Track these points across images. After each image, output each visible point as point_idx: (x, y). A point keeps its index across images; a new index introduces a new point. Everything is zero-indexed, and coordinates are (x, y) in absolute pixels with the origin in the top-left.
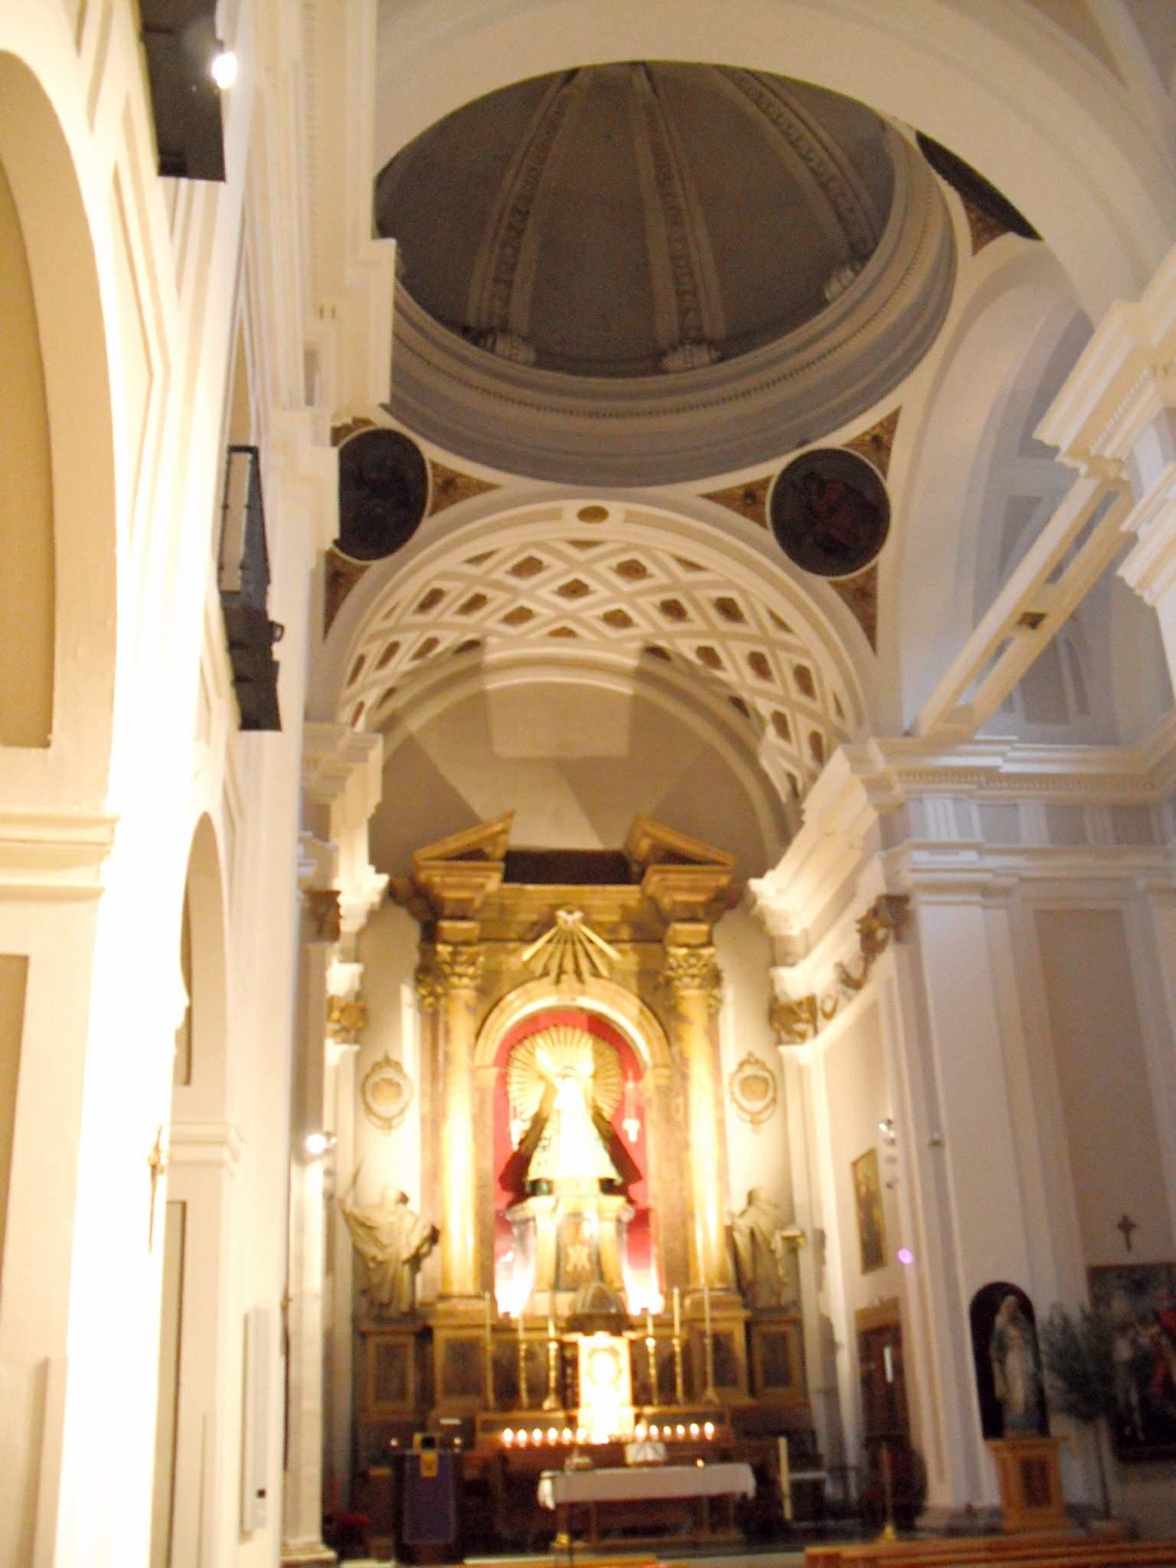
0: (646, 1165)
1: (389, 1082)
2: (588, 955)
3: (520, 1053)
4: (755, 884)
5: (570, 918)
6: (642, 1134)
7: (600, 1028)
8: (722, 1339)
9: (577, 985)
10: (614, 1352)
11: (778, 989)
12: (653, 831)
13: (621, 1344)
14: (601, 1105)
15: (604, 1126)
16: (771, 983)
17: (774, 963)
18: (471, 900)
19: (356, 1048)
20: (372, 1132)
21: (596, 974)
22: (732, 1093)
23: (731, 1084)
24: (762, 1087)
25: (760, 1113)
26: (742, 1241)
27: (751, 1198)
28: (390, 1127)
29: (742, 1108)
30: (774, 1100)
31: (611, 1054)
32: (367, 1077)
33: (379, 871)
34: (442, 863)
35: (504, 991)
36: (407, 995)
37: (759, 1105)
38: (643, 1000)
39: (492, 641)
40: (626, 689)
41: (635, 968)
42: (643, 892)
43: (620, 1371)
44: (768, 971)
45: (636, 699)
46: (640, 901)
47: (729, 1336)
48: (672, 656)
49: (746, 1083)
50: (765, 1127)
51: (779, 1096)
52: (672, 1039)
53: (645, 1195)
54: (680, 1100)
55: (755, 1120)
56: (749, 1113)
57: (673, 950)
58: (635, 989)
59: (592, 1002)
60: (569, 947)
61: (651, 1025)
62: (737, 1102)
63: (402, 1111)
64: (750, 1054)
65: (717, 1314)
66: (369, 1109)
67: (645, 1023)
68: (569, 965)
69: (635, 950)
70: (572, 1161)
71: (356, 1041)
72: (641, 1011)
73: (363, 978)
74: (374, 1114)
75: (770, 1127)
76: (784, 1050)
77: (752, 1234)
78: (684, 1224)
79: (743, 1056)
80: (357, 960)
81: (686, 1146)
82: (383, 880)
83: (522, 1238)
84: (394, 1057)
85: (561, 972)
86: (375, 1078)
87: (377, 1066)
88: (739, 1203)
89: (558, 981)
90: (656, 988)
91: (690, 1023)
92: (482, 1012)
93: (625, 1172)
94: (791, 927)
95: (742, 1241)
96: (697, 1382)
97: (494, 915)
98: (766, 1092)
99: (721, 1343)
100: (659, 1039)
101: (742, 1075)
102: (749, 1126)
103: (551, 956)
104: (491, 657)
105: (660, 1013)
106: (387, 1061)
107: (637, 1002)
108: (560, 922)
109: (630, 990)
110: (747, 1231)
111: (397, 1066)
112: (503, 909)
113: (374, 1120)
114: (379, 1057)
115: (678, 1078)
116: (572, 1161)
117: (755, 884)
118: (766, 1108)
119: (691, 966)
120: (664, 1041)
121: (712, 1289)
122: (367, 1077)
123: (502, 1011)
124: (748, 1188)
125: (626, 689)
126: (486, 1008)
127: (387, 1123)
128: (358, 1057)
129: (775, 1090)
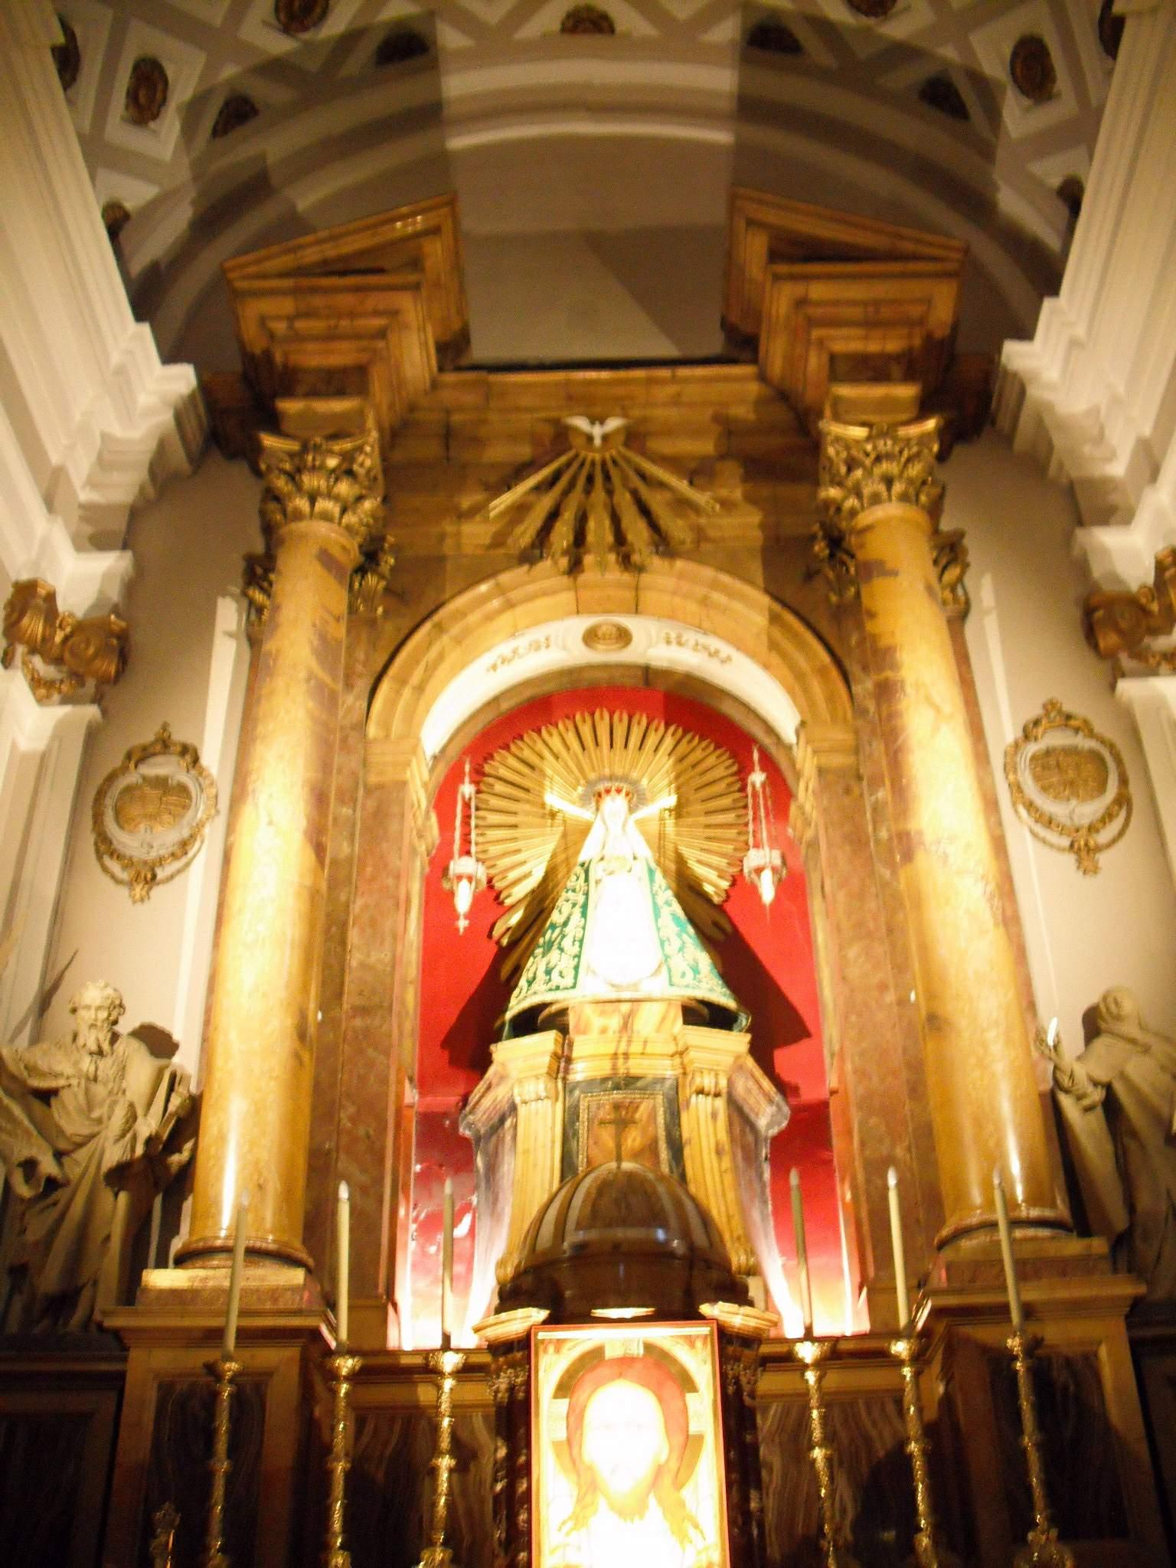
0: (814, 1000)
1: (161, 783)
2: (645, 511)
3: (504, 765)
4: (1015, 354)
5: (597, 431)
6: (793, 886)
7: (692, 711)
8: (1060, 1376)
9: (615, 574)
10: (663, 1373)
11: (1097, 572)
12: (772, 217)
13: (690, 1348)
14: (700, 870)
15: (705, 914)
16: (1081, 568)
17: (1080, 523)
18: (262, 157)
19: (92, 711)
20: (104, 896)
21: (664, 545)
22: (1016, 788)
23: (1010, 767)
24: (1089, 769)
25: (1092, 829)
26: (1086, 1126)
27: (1094, 1024)
28: (152, 880)
29: (1049, 822)
30: (1123, 800)
31: (718, 765)
32: (111, 778)
33: (170, 355)
34: (288, 283)
35: (447, 596)
36: (228, 614)
37: (1088, 810)
38: (776, 598)
39: (450, 38)
40: (721, 136)
41: (756, 537)
42: (762, 378)
43: (689, 1444)
44: (1068, 538)
45: (740, 150)
46: (760, 403)
47: (1084, 1367)
48: (803, 34)
49: (1047, 764)
50: (1103, 858)
51: (1135, 789)
52: (854, 669)
53: (818, 1073)
54: (883, 794)
55: (1084, 851)
56: (1062, 830)
57: (833, 429)
58: (760, 579)
59: (660, 644)
60: (599, 494)
61: (801, 645)
62: (1030, 806)
63: (184, 845)
64: (1050, 706)
65: (1032, 1295)
66: (105, 847)
67: (788, 646)
68: (599, 529)
69: (749, 499)
70: (624, 961)
71: (98, 699)
72: (774, 619)
73: (132, 587)
74: (114, 854)
75: (1122, 860)
76: (1128, 688)
77: (1111, 1107)
78: (916, 1089)
79: (1037, 711)
80: (125, 546)
81: (905, 846)
82: (183, 378)
83: (492, 1168)
84: (179, 735)
85: (579, 539)
86: (132, 778)
87: (143, 754)
88: (1061, 1024)
89: (575, 567)
90: (810, 576)
91: (894, 573)
92: (390, 631)
93: (755, 992)
94: (1111, 457)
95: (1086, 1126)
96: (989, 1521)
97: (431, 449)
98: (1102, 788)
99: (1063, 1385)
100: (822, 672)
101: (1032, 748)
102: (1070, 859)
103: (554, 515)
104: (459, 85)
105: (824, 626)
106: (164, 744)
107: (765, 600)
108: (578, 442)
109: (750, 582)
110: (1097, 1095)
111: (190, 754)
112: (448, 435)
113: (115, 866)
114: (147, 735)
115: (878, 748)
116: (624, 961)
117: (1015, 354)
118: (1108, 817)
119: (878, 459)
120: (834, 673)
121: (1015, 1223)
122: (111, 778)
123: (440, 628)
124: (1092, 999)
125: (721, 136)
126: (406, 624)
127: (146, 876)
128: (93, 738)
129: (1123, 781)
